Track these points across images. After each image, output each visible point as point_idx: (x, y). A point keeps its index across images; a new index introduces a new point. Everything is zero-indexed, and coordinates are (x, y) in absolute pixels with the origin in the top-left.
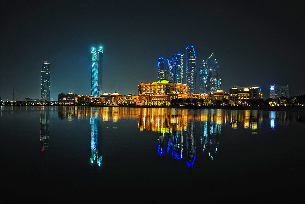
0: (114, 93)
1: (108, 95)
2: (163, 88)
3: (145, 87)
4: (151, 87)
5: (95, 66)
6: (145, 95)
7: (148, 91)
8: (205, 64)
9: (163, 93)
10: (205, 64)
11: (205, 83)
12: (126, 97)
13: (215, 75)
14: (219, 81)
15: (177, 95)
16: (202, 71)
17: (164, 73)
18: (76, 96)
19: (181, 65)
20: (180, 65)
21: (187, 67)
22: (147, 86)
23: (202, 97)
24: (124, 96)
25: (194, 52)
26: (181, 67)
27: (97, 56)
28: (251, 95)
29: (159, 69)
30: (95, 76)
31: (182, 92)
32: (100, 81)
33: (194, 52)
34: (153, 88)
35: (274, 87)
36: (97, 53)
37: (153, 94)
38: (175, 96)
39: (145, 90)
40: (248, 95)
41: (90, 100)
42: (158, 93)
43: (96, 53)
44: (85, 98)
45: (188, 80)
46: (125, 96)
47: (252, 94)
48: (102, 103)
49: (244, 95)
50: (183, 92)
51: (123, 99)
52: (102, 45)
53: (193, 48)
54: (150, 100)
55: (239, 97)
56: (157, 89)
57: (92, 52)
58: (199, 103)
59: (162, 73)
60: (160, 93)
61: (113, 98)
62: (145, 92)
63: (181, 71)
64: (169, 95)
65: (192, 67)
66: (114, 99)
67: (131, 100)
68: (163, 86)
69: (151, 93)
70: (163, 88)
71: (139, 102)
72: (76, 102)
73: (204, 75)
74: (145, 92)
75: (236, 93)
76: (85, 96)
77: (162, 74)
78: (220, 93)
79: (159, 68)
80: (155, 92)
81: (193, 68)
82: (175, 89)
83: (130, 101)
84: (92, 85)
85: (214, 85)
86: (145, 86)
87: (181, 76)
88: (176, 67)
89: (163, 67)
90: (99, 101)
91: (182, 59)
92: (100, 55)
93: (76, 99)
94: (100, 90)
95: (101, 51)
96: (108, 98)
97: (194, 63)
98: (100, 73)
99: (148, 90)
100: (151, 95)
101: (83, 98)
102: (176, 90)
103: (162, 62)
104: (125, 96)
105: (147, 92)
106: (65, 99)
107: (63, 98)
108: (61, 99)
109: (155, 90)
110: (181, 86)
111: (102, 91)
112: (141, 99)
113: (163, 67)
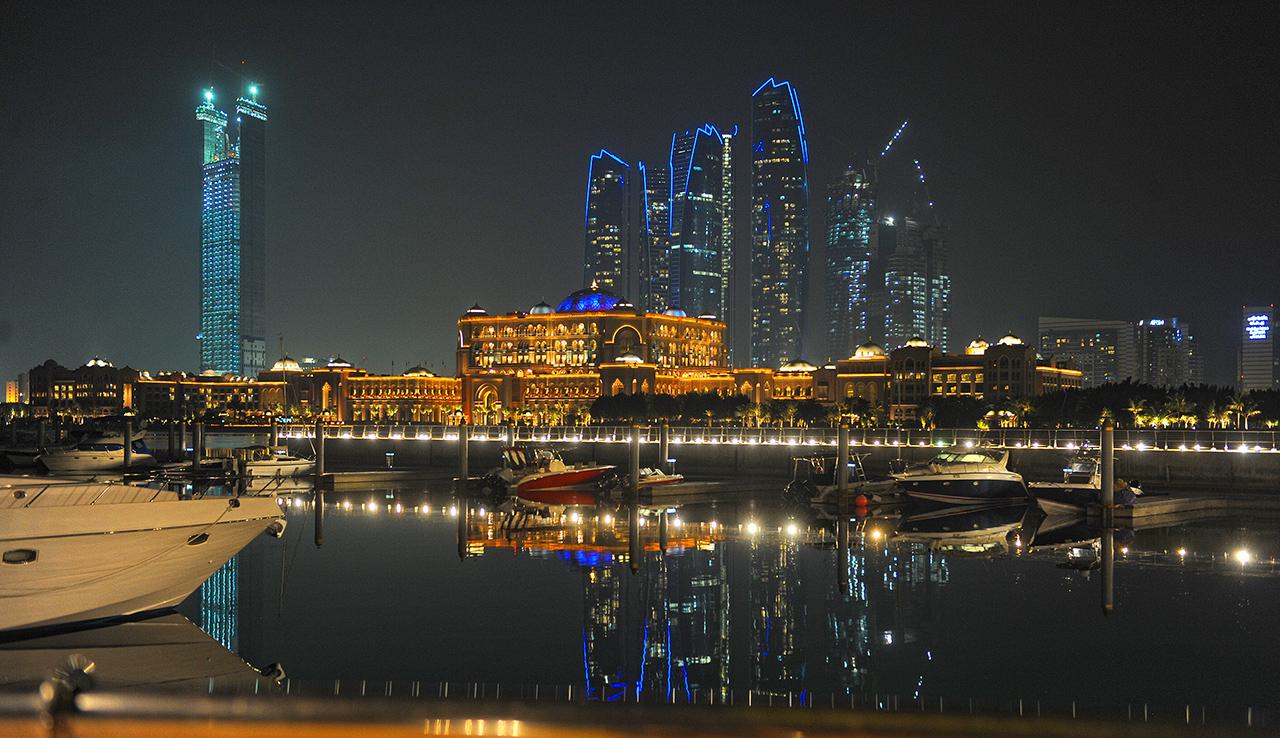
0: (330, 365)
1: (299, 373)
2: (586, 336)
3: (491, 330)
4: (522, 330)
5: (219, 201)
6: (492, 371)
7: (509, 352)
8: (858, 185)
9: (584, 365)
10: (858, 185)
11: (855, 297)
12: (395, 382)
13: (911, 250)
14: (937, 286)
15: (647, 374)
16: (842, 229)
17: (617, 242)
18: (127, 375)
19: (718, 195)
20: (711, 196)
21: (756, 202)
22: (503, 325)
23: (780, 382)
24: (384, 378)
25: (798, 114)
26: (720, 206)
27: (233, 140)
28: (989, 377)
29: (589, 216)
30: (221, 260)
31: (688, 357)
32: (251, 287)
33: (798, 114)
34: (532, 338)
35: (1265, 318)
36: (228, 119)
37: (530, 371)
38: (635, 381)
39: (491, 345)
40: (949, 376)
41: (203, 397)
42: (561, 362)
43: (225, 123)
44: (173, 390)
45: (760, 278)
46: (388, 378)
47: (995, 375)
48: (269, 414)
49: (959, 378)
50: (695, 357)
51: (377, 393)
52: (257, 80)
53: (793, 95)
54: (516, 399)
55: (939, 385)
56: (554, 341)
57: (200, 117)
58: (713, 417)
59: (607, 238)
60: (567, 365)
61: (326, 388)
62: (491, 359)
63: (718, 231)
64: (609, 376)
65: (785, 201)
66: (330, 394)
67: (416, 402)
68: (581, 326)
69: (523, 365)
70: (586, 336)
71: (459, 408)
72: (128, 410)
73: (856, 250)
74: (491, 359)
75: (921, 367)
76: (177, 376)
77: (608, 246)
78: (867, 362)
79: (591, 213)
80: (544, 357)
81: (790, 211)
82: (649, 340)
83: (411, 402)
84: (202, 312)
85: (906, 312)
86: (494, 325)
87: (719, 257)
88: (688, 204)
89: (616, 204)
90: (250, 406)
91: (727, 158)
92: (248, 133)
93: (125, 391)
94: (251, 340)
95: (256, 108)
96: (301, 388)
97: (797, 182)
98: (251, 240)
99: (510, 345)
100: (520, 374)
101: (166, 388)
102: (650, 344)
103: (609, 176)
104: (388, 378)
105: (504, 358)
106: (59, 392)
107: (57, 388)
108: (46, 390)
109: (542, 345)
110: (681, 327)
111: (263, 343)
112: (468, 397)
113: (616, 204)
